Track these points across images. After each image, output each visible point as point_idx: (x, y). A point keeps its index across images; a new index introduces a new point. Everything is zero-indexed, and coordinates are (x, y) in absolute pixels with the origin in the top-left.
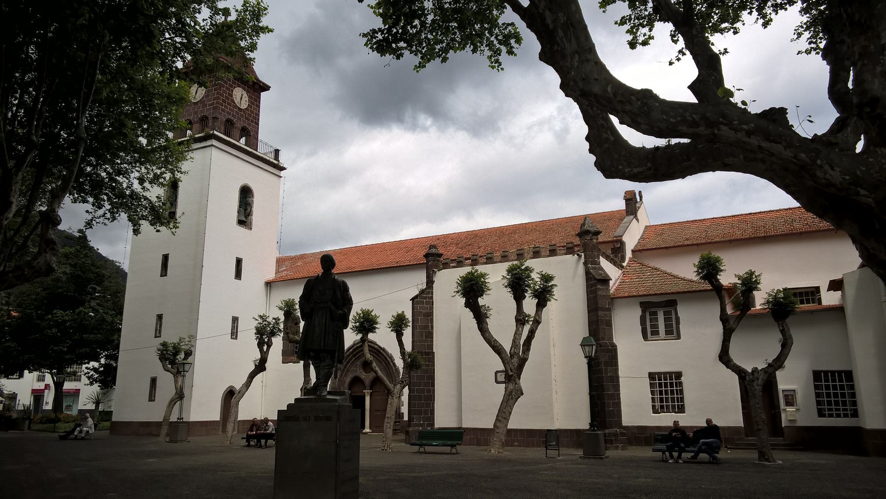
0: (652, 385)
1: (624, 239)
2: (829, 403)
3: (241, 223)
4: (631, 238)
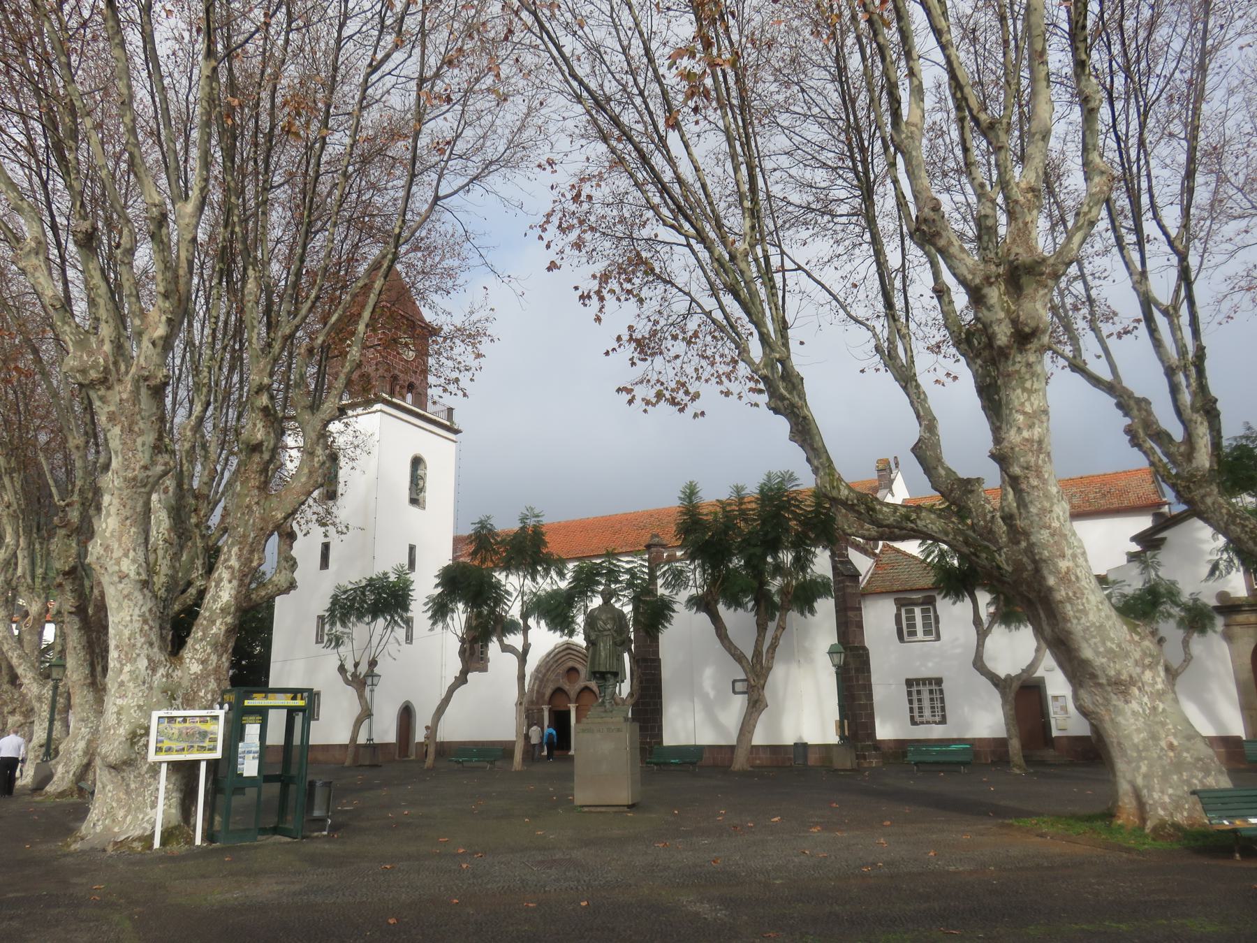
0: (910, 693)
3: (414, 501)
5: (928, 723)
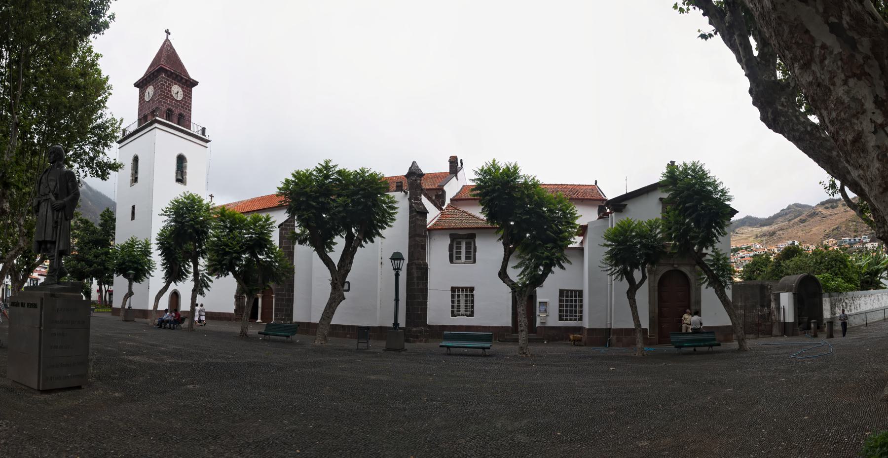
0: (453, 296)
1: (445, 188)
2: (567, 311)
3: (178, 180)
4: (452, 189)
5: (462, 315)
